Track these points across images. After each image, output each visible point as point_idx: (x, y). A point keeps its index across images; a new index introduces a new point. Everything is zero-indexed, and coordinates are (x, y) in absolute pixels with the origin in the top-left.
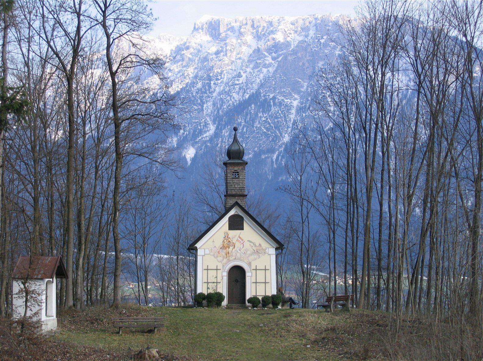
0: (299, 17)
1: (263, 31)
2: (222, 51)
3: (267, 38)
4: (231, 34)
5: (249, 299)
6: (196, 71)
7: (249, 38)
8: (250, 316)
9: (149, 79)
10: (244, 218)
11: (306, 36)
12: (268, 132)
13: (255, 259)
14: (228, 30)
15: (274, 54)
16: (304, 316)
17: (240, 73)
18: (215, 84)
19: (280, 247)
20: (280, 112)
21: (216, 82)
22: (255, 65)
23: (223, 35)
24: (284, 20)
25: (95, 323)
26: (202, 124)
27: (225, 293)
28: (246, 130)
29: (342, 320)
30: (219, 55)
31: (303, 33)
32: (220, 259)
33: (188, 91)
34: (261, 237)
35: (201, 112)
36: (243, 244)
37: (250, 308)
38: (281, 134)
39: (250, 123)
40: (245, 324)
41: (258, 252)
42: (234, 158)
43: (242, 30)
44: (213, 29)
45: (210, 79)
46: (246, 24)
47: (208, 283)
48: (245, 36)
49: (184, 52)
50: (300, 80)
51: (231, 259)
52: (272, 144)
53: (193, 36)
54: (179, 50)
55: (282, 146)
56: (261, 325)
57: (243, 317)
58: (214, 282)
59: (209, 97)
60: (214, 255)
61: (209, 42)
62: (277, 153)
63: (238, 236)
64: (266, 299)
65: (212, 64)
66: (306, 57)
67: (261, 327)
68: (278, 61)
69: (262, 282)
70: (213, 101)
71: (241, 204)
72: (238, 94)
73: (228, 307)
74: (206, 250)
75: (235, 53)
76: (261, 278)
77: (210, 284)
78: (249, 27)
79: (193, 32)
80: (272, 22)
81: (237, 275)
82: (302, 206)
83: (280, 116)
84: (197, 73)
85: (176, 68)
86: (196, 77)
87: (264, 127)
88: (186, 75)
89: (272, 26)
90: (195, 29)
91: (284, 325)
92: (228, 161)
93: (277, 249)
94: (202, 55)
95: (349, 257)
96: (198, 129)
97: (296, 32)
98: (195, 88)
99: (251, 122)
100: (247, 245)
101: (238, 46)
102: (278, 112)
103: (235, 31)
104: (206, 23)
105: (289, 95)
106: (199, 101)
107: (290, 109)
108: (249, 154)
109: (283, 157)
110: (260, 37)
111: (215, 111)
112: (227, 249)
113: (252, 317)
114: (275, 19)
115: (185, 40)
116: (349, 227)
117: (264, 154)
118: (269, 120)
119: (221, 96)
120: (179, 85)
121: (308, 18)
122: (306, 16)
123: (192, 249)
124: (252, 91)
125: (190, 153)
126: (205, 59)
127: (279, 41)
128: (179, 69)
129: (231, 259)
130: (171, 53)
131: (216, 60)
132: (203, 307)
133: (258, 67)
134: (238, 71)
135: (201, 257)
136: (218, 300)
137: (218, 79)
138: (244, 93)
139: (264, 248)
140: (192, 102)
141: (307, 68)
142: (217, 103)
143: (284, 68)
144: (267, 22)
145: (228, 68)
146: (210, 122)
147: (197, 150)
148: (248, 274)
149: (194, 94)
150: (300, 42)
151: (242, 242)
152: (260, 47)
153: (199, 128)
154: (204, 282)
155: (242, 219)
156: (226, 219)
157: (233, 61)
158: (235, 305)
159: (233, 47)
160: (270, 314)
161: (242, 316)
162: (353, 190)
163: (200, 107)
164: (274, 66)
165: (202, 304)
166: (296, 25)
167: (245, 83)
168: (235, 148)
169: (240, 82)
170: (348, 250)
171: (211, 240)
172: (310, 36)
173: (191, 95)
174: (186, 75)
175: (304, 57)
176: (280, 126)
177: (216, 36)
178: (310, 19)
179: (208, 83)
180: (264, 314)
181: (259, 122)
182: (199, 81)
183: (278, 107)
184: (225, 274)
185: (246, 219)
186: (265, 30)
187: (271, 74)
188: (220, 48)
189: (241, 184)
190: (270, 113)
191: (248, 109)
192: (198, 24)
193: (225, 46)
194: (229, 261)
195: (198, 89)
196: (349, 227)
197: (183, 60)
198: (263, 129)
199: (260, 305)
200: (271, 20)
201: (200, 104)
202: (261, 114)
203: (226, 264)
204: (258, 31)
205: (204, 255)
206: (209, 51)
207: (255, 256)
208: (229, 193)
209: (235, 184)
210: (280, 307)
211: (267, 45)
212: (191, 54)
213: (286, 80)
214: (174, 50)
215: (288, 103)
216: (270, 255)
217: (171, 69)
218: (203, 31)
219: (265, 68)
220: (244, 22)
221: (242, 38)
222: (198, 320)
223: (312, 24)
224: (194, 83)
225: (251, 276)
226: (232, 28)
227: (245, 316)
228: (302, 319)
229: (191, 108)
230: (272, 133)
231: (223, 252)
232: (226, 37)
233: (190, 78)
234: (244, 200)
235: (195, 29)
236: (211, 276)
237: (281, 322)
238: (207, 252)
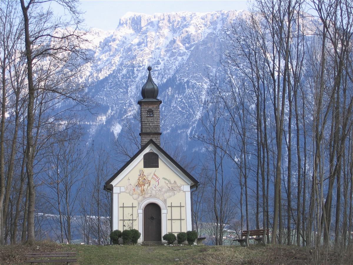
0: (207, 13)
1: (178, 25)
2: (143, 42)
3: (181, 31)
4: (151, 28)
5: (165, 236)
6: (121, 59)
7: (166, 31)
8: (166, 251)
11: (215, 29)
12: (183, 110)
13: (170, 197)
14: (148, 24)
15: (187, 45)
16: (220, 250)
17: (158, 61)
18: (137, 70)
19: (195, 185)
20: (193, 93)
21: (138, 68)
22: (171, 54)
23: (144, 29)
24: (195, 15)
25: (7, 260)
26: (127, 105)
27: (141, 230)
28: (165, 109)
29: (259, 254)
30: (141, 46)
31: (212, 27)
32: (135, 196)
33: (115, 77)
34: (164, 164)
35: (126, 94)
36: (158, 181)
37: (166, 245)
38: (194, 112)
39: (168, 103)
40: (160, 259)
41: (173, 189)
42: (148, 97)
43: (160, 24)
44: (136, 23)
45: (133, 67)
46: (164, 19)
47: (124, 220)
48: (163, 29)
50: (209, 66)
51: (146, 196)
52: (187, 121)
53: (119, 30)
55: (195, 123)
56: (176, 260)
57: (158, 253)
58: (130, 220)
59: (133, 82)
60: (129, 193)
61: (131, 35)
62: (191, 128)
63: (152, 175)
64: (182, 235)
65: (134, 53)
66: (214, 46)
67: (177, 261)
68: (190, 50)
69: (177, 219)
71: (156, 142)
72: (157, 79)
73: (144, 244)
74: (121, 187)
75: (154, 44)
76: (176, 216)
77: (125, 221)
78: (166, 21)
79: (118, 26)
80: (185, 17)
81: (153, 213)
82: (215, 155)
83: (193, 97)
84: (123, 61)
85: (104, 57)
86: (121, 64)
87: (180, 107)
88: (113, 63)
89: (186, 21)
90: (121, 24)
91: (200, 259)
92: (142, 99)
93: (191, 187)
94: (127, 46)
95: (261, 200)
96: (124, 109)
97: (206, 25)
99: (169, 102)
100: (162, 182)
101: (156, 38)
102: (191, 94)
103: (154, 25)
104: (130, 19)
105: (200, 79)
106: (124, 85)
107: (202, 91)
108: (167, 129)
109: (196, 132)
110: (176, 30)
111: (138, 93)
112: (142, 187)
113: (168, 252)
114: (188, 14)
115: (112, 34)
116: (260, 171)
117: (180, 129)
118: (183, 100)
119: (143, 81)
120: (107, 72)
121: (216, 14)
122: (214, 12)
123: (109, 188)
124: (169, 76)
125: (117, 129)
126: (130, 49)
127: (192, 33)
129: (146, 196)
131: (138, 50)
132: (120, 245)
133: (174, 56)
134: (157, 59)
135: (117, 194)
136: (133, 237)
137: (140, 67)
138: (163, 77)
139: (179, 185)
140: (118, 85)
141: (215, 56)
142: (140, 87)
143: (196, 56)
144: (181, 17)
145: (148, 57)
146: (133, 103)
147: (123, 126)
148: (163, 211)
149: (120, 79)
150: (209, 34)
151: (157, 180)
152: (175, 38)
153: (125, 107)
155: (157, 156)
156: (141, 157)
157: (153, 51)
158: (150, 243)
159: (152, 39)
160: (186, 249)
161: (158, 251)
162: (263, 135)
163: (125, 90)
164: (187, 54)
165: (118, 241)
166: (206, 20)
167: (163, 69)
168: (150, 87)
169: (159, 68)
170: (259, 192)
171: (127, 177)
172: (218, 29)
173: (117, 80)
174: (113, 63)
175: (213, 47)
176: (193, 105)
177: (138, 30)
178: (218, 14)
179: (131, 70)
180: (179, 249)
181: (175, 102)
182: (124, 68)
183: (191, 89)
184: (141, 211)
185: (161, 157)
186: (179, 24)
187: (185, 62)
188: (142, 40)
189: (155, 122)
190: (185, 95)
191: (166, 91)
192: (123, 19)
193: (145, 38)
194: (144, 198)
195: (123, 75)
196: (260, 171)
197: (110, 50)
198: (179, 108)
199: (176, 242)
200: (184, 16)
201: (125, 88)
202: (177, 95)
203: (142, 201)
204: (173, 25)
205: (120, 193)
206: (132, 43)
208: (143, 131)
209: (149, 122)
210: (195, 244)
211: (182, 37)
213: (197, 66)
214: (103, 41)
215: (200, 86)
216: (185, 192)
217: (100, 58)
218: (127, 26)
219: (180, 56)
220: (162, 18)
221: (160, 31)
222: (113, 255)
223: (219, 19)
224: (120, 70)
226: (152, 22)
227: (161, 252)
228: (218, 253)
229: (118, 91)
230: (186, 111)
231: (139, 190)
232: (147, 31)
233: (116, 66)
234: (159, 138)
235: (121, 24)
236: (126, 212)
237: (197, 256)
238: (123, 189)
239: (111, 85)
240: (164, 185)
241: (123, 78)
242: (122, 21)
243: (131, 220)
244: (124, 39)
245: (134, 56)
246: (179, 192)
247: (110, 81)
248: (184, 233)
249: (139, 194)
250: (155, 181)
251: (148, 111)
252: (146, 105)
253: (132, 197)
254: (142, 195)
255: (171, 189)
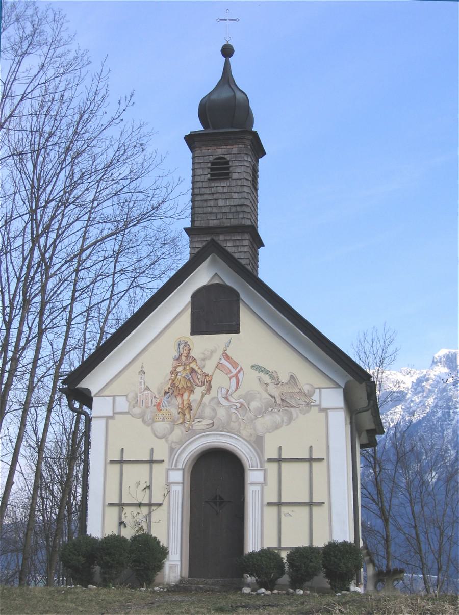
6: (436, 401)
9: (393, 409)
10: (242, 296)
13: (277, 427)
18: (454, 412)
32: (162, 426)
33: (429, 420)
34: (279, 340)
36: (236, 376)
41: (288, 401)
45: (449, 408)
47: (121, 505)
49: (424, 384)
51: (197, 426)
53: (432, 369)
54: (419, 382)
58: (140, 505)
60: (142, 416)
63: (220, 352)
65: (451, 394)
70: (453, 428)
71: (236, 256)
74: (117, 398)
79: (432, 365)
81: (218, 481)
84: (437, 403)
85: (417, 399)
86: (436, 406)
88: (426, 404)
90: (434, 363)
98: (436, 417)
104: (444, 357)
106: (440, 429)
111: (455, 437)
112: (186, 396)
115: (425, 373)
120: (421, 415)
126: (444, 390)
128: (420, 399)
129: (197, 426)
130: (412, 385)
131: (454, 390)
139: (306, 388)
148: (253, 477)
149: (435, 423)
151: (234, 372)
154: (108, 501)
156: (182, 299)
163: (440, 434)
171: (137, 367)
174: (426, 404)
179: (447, 412)
184: (177, 476)
189: (236, 196)
194: (191, 433)
195: (438, 418)
199: (285, 579)
201: (440, 432)
203: (181, 443)
205: (112, 418)
207: (278, 418)
209: (215, 196)
212: (431, 385)
214: (415, 382)
216: (326, 410)
217: (413, 400)
218: (441, 364)
224: (434, 412)
225: (264, 484)
231: (172, 408)
233: (430, 408)
238: (122, 404)
239: (425, 429)
240: (257, 387)
241: (437, 421)
242: (436, 358)
243: (145, 505)
244: (438, 378)
245: (450, 397)
246: (308, 411)
247: (424, 425)
248: (317, 549)
249: (174, 421)
250: (227, 377)
251: (213, 164)
252: (206, 146)
253: (149, 428)
254: (183, 422)
255: (279, 401)
